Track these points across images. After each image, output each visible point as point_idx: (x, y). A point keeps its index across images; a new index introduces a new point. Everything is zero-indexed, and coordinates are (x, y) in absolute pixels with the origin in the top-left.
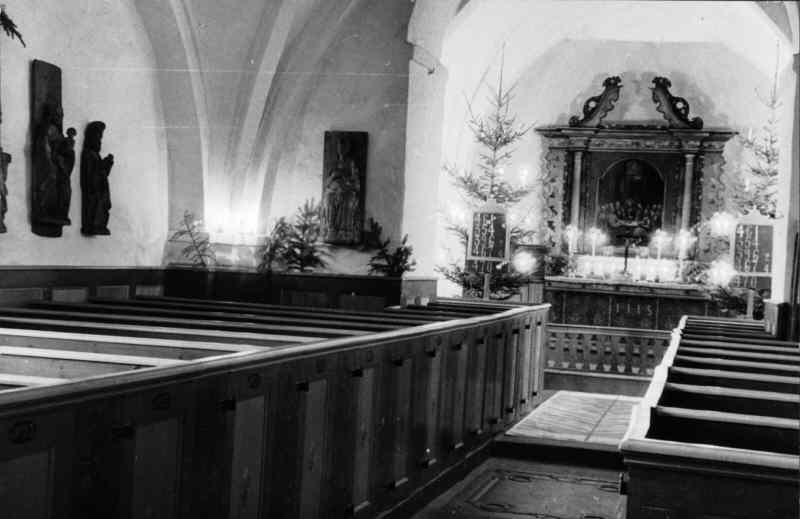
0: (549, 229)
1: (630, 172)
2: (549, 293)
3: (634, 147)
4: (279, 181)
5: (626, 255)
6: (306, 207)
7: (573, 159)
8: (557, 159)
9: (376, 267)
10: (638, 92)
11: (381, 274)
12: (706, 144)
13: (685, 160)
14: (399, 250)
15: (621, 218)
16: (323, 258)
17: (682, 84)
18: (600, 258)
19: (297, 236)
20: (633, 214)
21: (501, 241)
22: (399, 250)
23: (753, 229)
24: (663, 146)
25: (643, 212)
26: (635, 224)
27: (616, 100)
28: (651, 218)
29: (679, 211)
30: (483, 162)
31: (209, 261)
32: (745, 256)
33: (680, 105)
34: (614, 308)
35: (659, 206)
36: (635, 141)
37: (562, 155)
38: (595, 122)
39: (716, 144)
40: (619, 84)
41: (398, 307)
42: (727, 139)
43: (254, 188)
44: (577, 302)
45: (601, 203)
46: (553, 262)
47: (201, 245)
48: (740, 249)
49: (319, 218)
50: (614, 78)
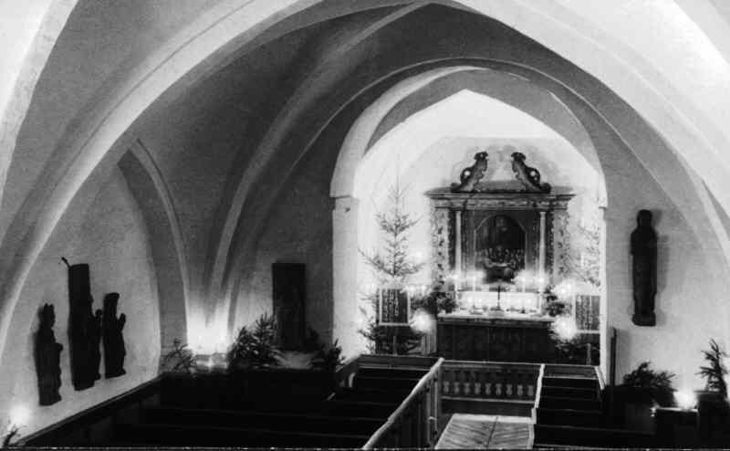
0: (439, 270)
1: (498, 225)
3: (501, 206)
4: (240, 299)
5: (499, 290)
6: (262, 320)
7: (455, 216)
8: (443, 216)
9: (315, 365)
10: (501, 160)
11: (319, 369)
12: (554, 203)
13: (540, 216)
14: (331, 351)
15: (493, 260)
16: (277, 357)
17: (533, 155)
18: (479, 293)
19: (255, 341)
20: (503, 257)
21: (404, 311)
22: (331, 351)
23: (588, 299)
24: (523, 205)
25: (510, 255)
26: (504, 265)
27: (485, 170)
28: (516, 260)
29: (537, 254)
30: (387, 246)
31: (192, 370)
32: (583, 318)
33: (533, 174)
34: (491, 337)
35: (522, 251)
37: (446, 212)
38: (469, 187)
39: (561, 203)
43: (222, 316)
44: (463, 337)
45: (478, 250)
46: (438, 301)
47: (187, 360)
48: (579, 312)
49: (272, 328)
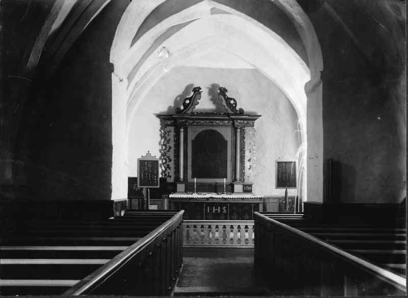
2: (172, 203)
33: (232, 102)
36: (211, 121)
40: (201, 91)
41: (113, 218)
42: (255, 119)
50: (197, 87)
